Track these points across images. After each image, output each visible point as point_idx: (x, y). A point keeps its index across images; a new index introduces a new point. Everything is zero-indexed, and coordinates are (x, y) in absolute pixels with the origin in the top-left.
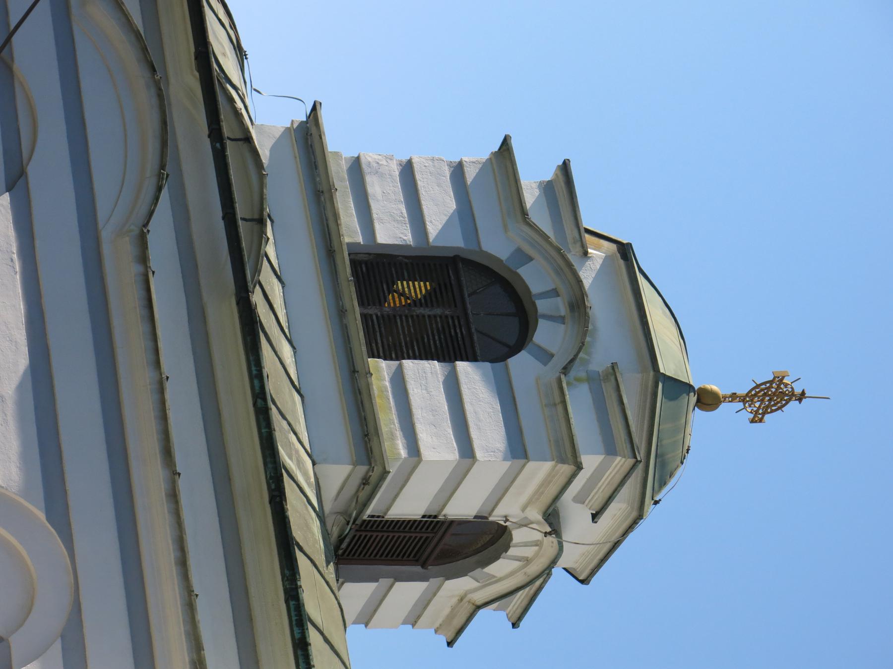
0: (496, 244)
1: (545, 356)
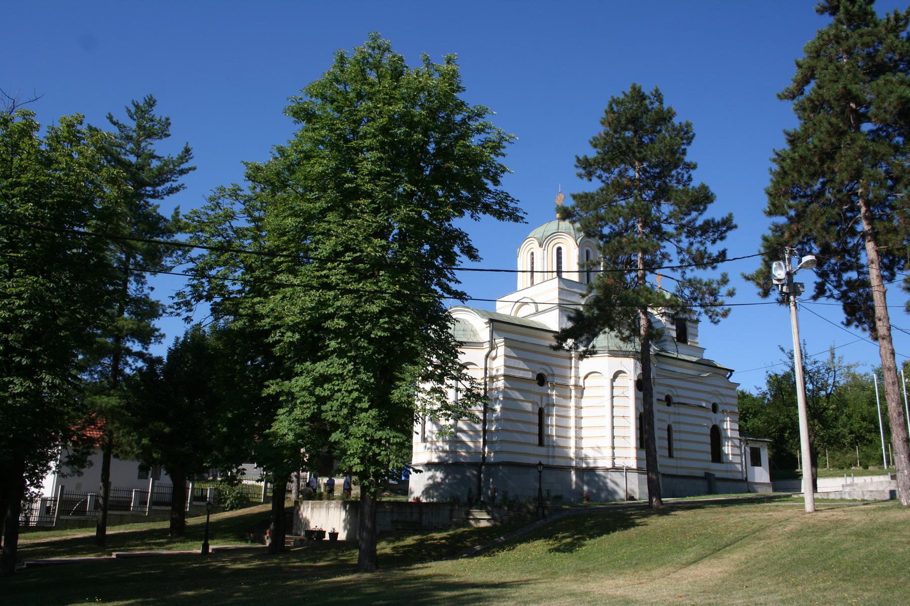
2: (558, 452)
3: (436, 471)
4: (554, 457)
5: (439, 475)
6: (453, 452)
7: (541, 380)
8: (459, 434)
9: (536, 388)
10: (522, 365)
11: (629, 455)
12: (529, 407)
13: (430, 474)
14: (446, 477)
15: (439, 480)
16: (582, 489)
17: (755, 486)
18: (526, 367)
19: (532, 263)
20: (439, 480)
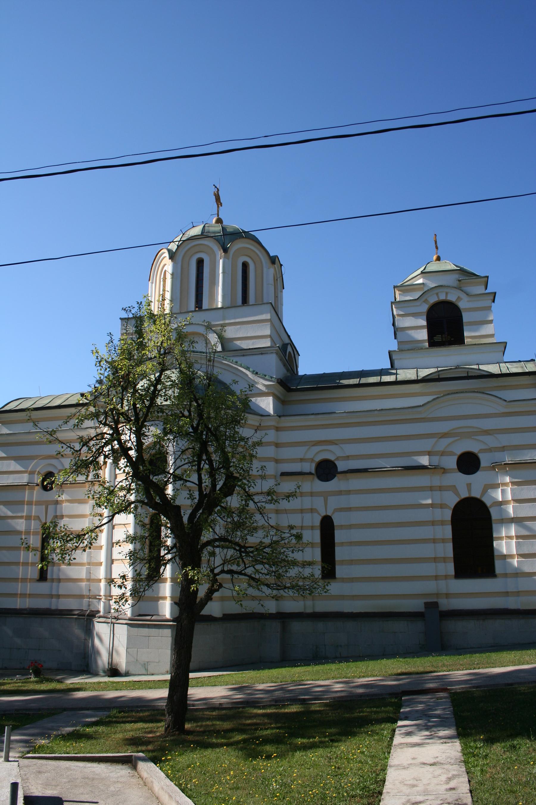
0: (425, 308)
1: (459, 298)
4: (58, 596)
9: (37, 493)
10: (13, 466)
18: (19, 468)
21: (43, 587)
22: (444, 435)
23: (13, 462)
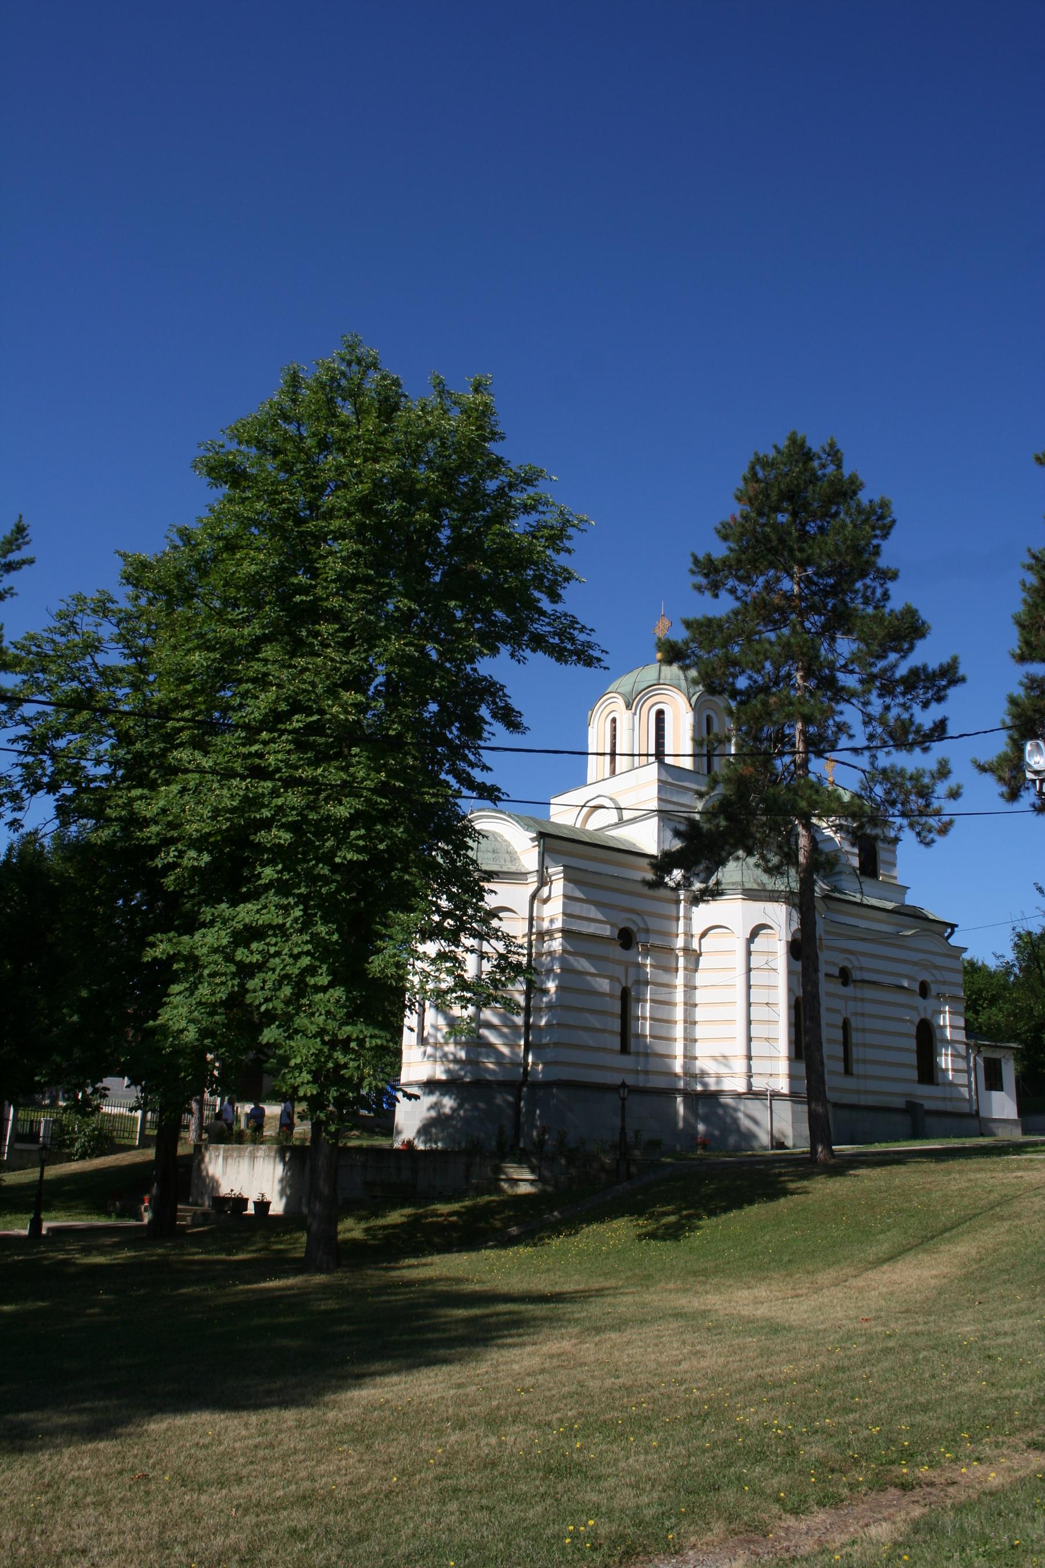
2: (653, 1064)
3: (443, 1094)
4: (646, 1072)
5: (448, 1103)
6: (471, 1062)
7: (626, 939)
8: (484, 1032)
9: (616, 951)
10: (593, 912)
11: (776, 1072)
12: (604, 985)
13: (432, 1099)
14: (460, 1106)
15: (447, 1110)
16: (695, 1128)
17: (993, 1125)
18: (600, 917)
19: (614, 737)
20: (447, 1110)
21: (626, 1061)
22: (915, 964)
23: (593, 908)
